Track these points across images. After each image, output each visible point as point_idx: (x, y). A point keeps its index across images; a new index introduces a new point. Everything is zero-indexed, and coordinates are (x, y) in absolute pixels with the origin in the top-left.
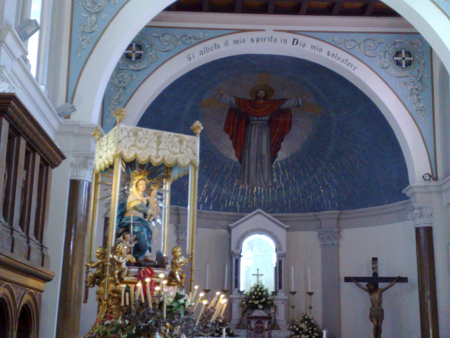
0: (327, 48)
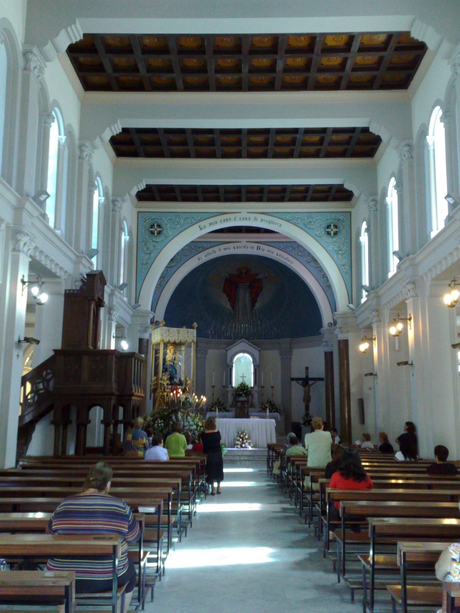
0: (276, 251)
